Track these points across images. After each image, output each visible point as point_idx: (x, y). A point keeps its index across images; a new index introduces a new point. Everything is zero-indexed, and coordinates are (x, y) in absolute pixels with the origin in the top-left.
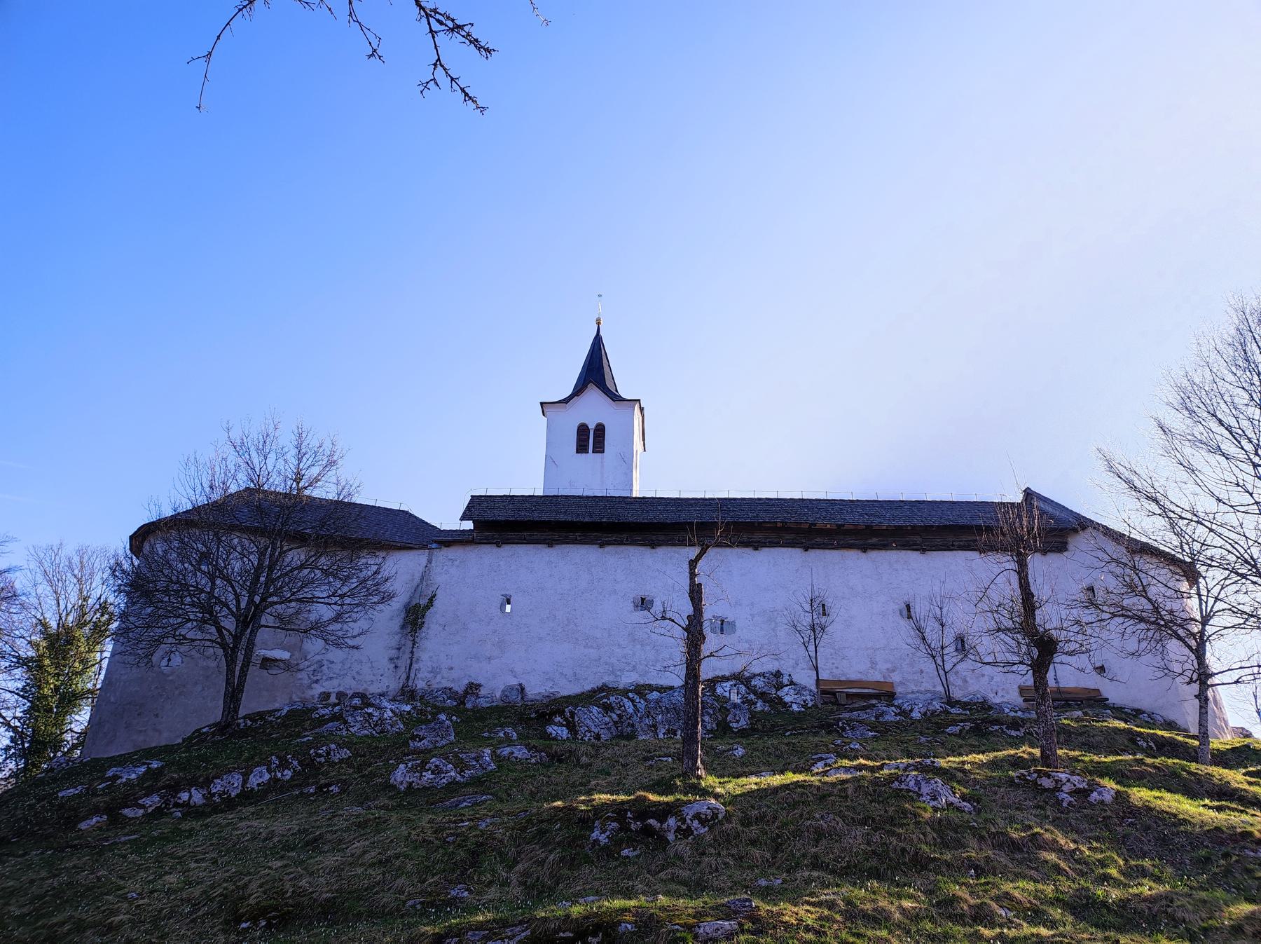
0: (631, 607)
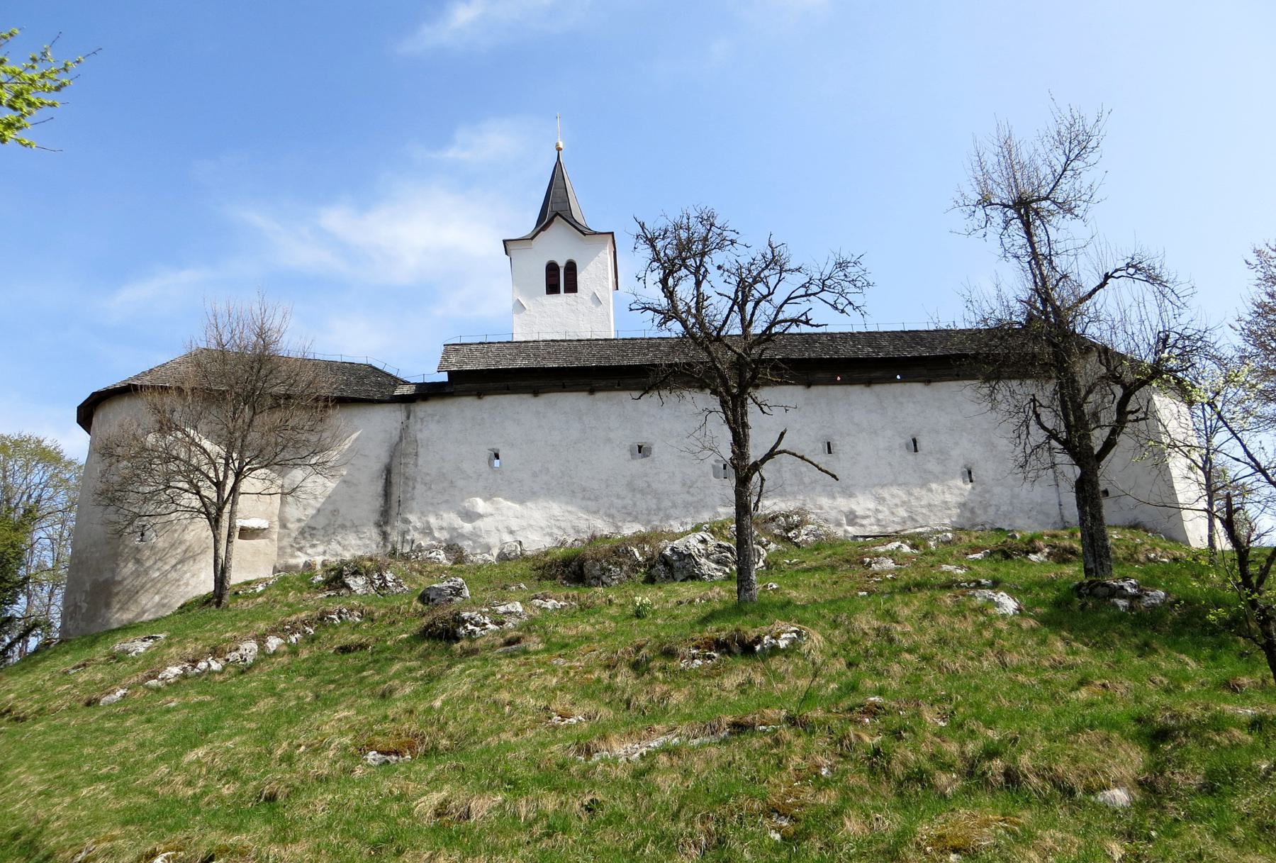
0: (628, 455)
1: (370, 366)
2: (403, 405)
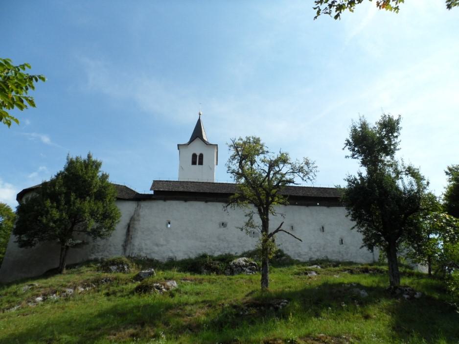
0: (218, 226)
1: (125, 186)
2: (136, 202)
